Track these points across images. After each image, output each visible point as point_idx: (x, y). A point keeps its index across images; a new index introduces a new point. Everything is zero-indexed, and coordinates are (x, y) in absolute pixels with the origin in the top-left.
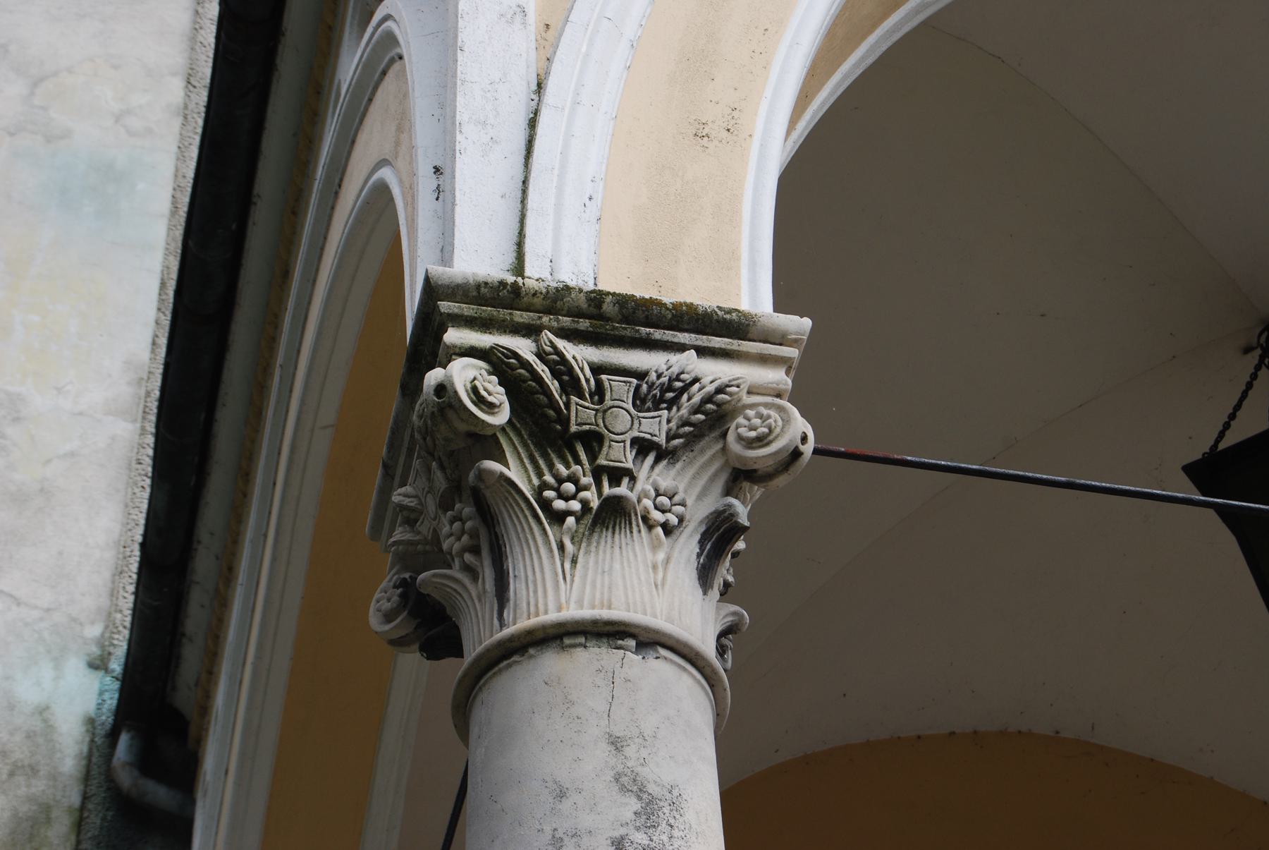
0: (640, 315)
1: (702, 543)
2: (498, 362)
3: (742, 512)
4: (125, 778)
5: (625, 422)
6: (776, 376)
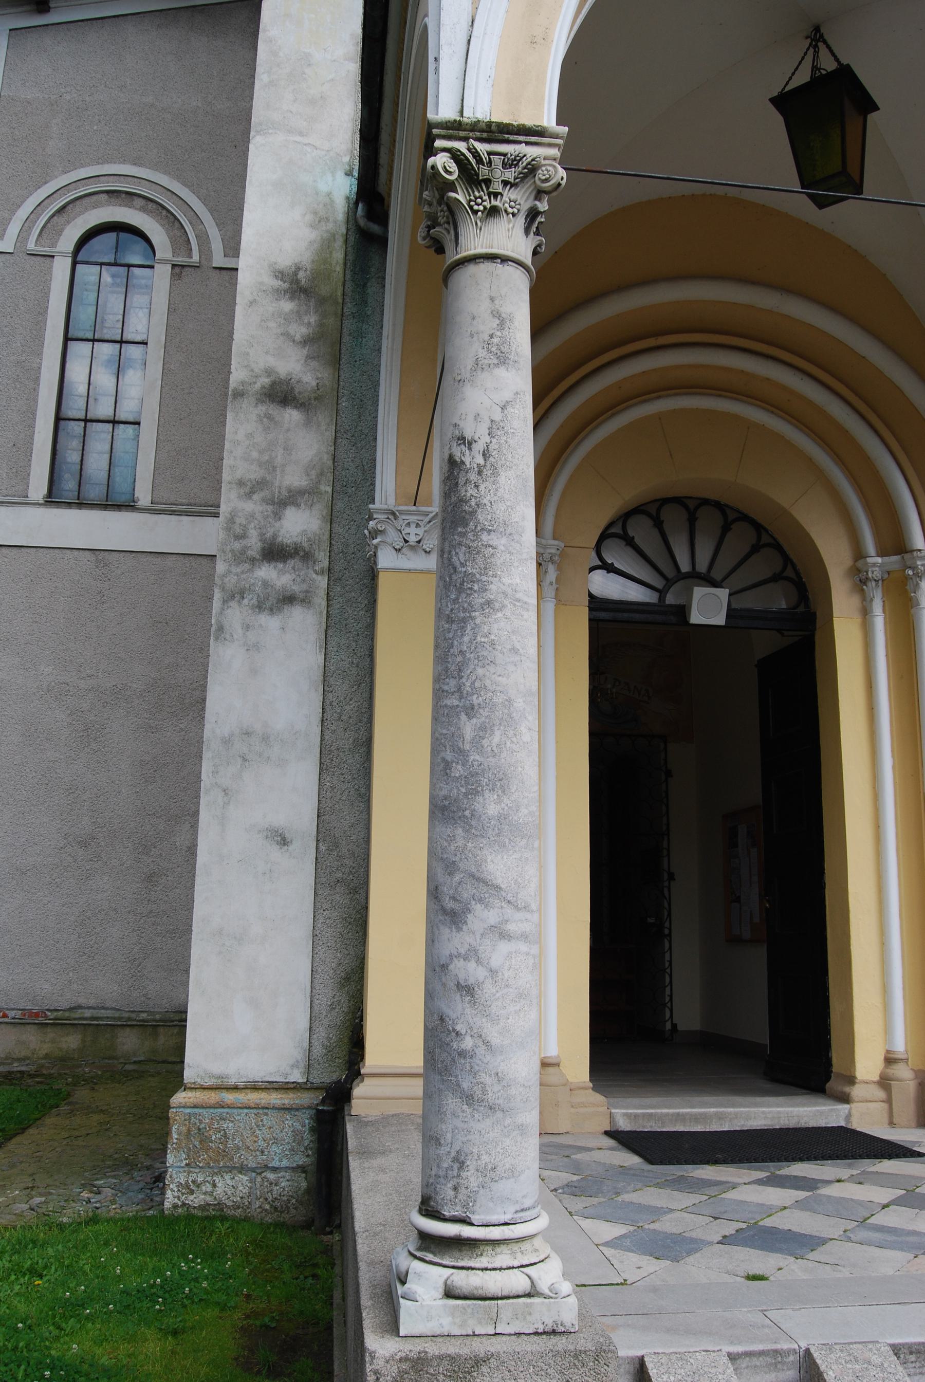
0: (505, 130)
1: (526, 219)
2: (455, 155)
3: (543, 206)
4: (362, 222)
5: (500, 174)
6: (555, 152)
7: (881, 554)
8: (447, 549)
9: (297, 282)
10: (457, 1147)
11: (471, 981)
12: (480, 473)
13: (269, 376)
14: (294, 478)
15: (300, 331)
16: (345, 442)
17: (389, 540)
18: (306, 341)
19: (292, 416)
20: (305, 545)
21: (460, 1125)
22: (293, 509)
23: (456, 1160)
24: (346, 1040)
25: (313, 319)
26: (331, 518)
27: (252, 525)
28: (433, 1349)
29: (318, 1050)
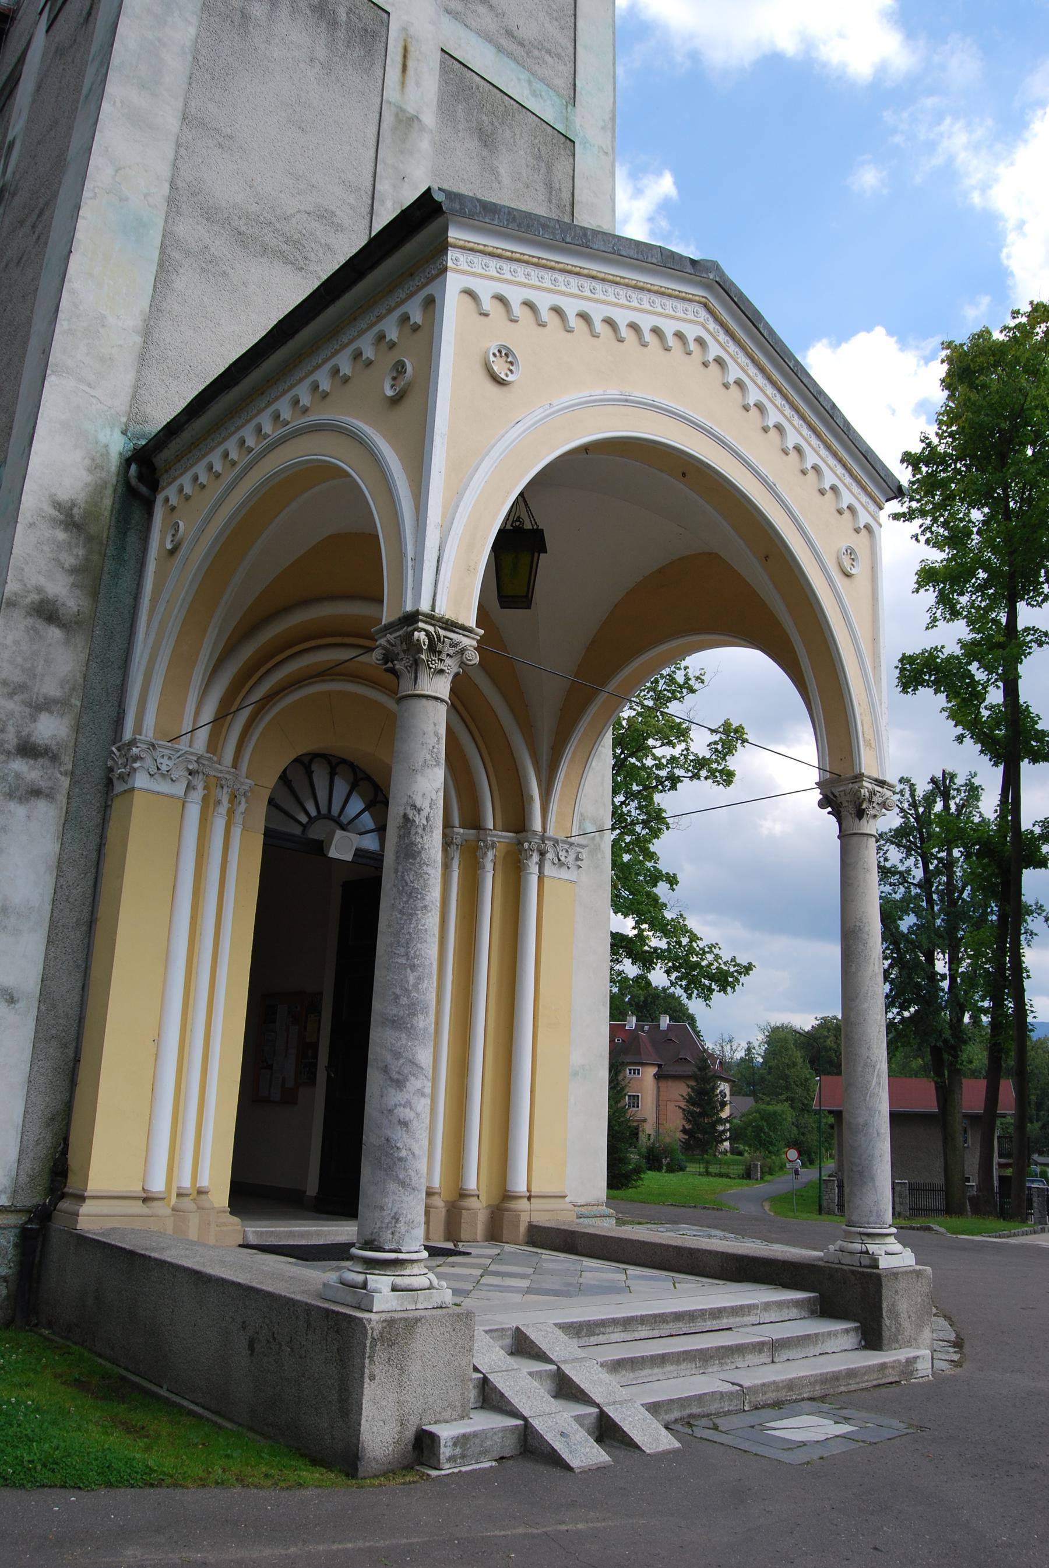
2: (428, 634)
4: (134, 482)
7: (463, 826)
8: (400, 869)
9: (72, 516)
10: (395, 1210)
11: (407, 1119)
12: (424, 829)
13: (39, 593)
14: (50, 688)
15: (69, 561)
16: (95, 665)
17: (146, 766)
18: (73, 571)
19: (55, 633)
20: (54, 748)
21: (396, 1197)
22: (47, 714)
23: (394, 1218)
24: (47, 1170)
25: (81, 552)
26: (78, 728)
27: (11, 722)
28: (397, 1316)
29: (24, 1179)
